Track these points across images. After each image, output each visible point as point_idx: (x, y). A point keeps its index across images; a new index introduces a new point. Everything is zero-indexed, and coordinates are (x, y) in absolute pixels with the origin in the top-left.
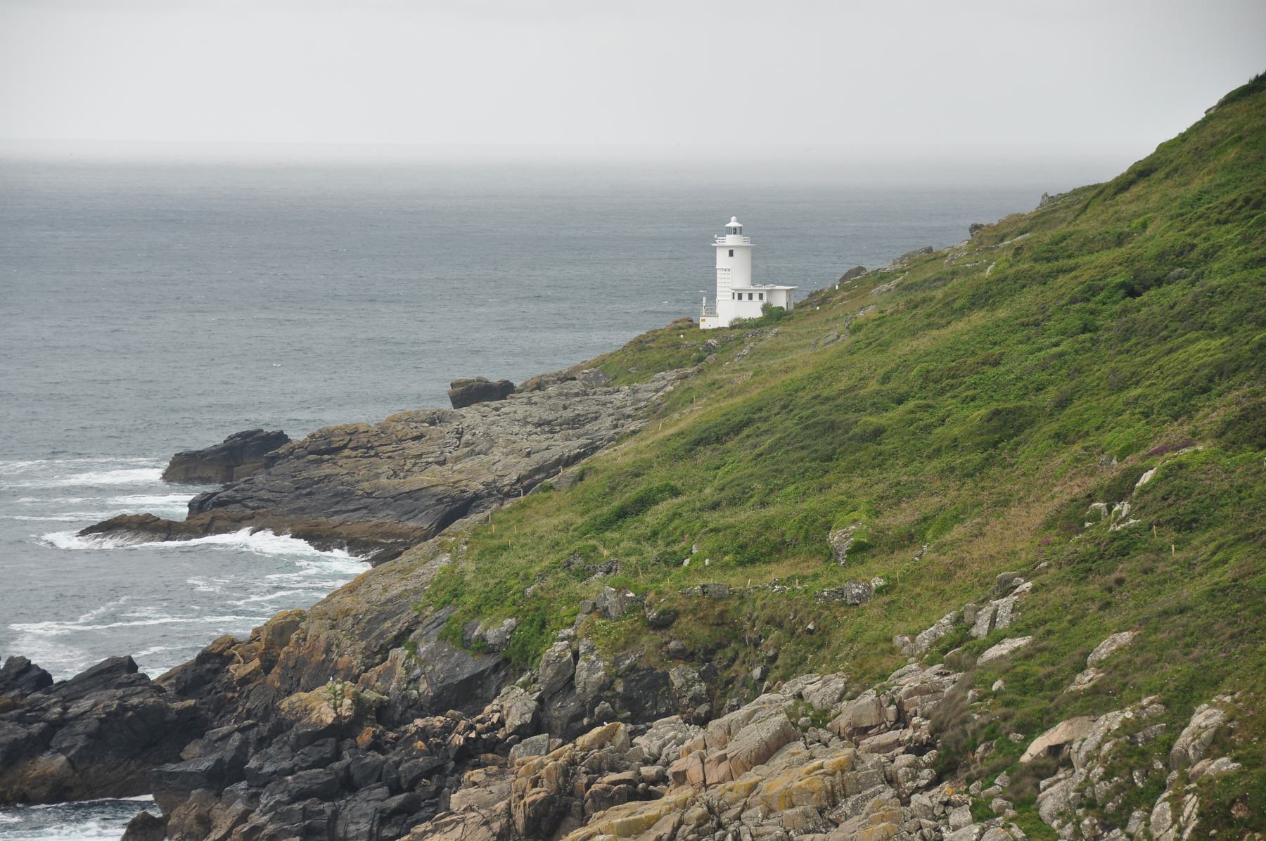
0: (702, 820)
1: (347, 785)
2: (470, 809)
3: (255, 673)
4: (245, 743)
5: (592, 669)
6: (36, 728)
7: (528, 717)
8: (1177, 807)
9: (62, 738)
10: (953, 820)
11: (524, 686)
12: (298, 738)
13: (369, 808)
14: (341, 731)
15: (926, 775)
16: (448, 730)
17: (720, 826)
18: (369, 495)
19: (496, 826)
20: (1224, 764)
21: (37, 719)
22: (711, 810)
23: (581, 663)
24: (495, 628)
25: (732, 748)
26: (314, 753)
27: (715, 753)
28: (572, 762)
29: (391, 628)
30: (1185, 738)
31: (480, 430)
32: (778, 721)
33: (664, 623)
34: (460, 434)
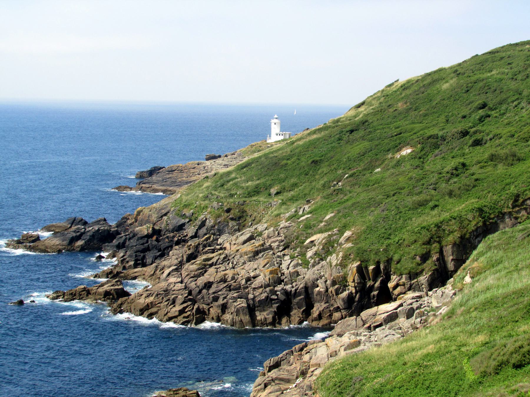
0: (224, 258)
1: (147, 249)
2: (173, 255)
3: (133, 223)
4: (126, 239)
5: (210, 222)
6: (78, 234)
7: (194, 234)
8: (337, 256)
9: (84, 237)
10: (285, 259)
11: (194, 226)
12: (138, 238)
13: (152, 255)
14: (149, 236)
15: (281, 248)
16: (174, 237)
17: (229, 260)
18: (180, 182)
19: (179, 260)
20: (350, 245)
21: (78, 232)
22: (227, 256)
23: (207, 220)
24: (188, 212)
25: (237, 241)
26: (141, 241)
27: (234, 242)
28: (199, 244)
29: (164, 212)
30: (341, 239)
31: (209, 167)
32: (248, 235)
33: (228, 211)
34: (205, 167)
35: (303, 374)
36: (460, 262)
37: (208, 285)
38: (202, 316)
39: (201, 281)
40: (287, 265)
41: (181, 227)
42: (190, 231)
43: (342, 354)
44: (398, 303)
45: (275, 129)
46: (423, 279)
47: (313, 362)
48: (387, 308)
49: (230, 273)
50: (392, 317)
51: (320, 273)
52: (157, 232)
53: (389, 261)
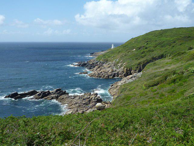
1: (92, 66)
35: (117, 87)
36: (143, 68)
37: (101, 72)
38: (100, 77)
39: (100, 71)
40: (114, 69)
41: (97, 63)
42: (99, 63)
43: (123, 83)
44: (133, 75)
45: (113, 46)
46: (137, 71)
47: (118, 85)
48: (131, 76)
49: (105, 70)
50: (132, 77)
51: (120, 70)
52: (93, 64)
53: (131, 68)
